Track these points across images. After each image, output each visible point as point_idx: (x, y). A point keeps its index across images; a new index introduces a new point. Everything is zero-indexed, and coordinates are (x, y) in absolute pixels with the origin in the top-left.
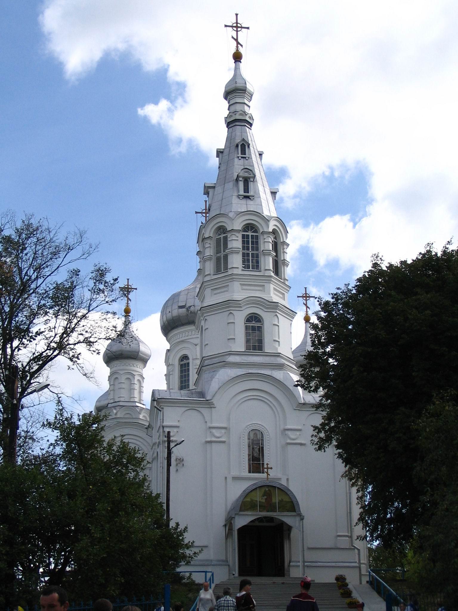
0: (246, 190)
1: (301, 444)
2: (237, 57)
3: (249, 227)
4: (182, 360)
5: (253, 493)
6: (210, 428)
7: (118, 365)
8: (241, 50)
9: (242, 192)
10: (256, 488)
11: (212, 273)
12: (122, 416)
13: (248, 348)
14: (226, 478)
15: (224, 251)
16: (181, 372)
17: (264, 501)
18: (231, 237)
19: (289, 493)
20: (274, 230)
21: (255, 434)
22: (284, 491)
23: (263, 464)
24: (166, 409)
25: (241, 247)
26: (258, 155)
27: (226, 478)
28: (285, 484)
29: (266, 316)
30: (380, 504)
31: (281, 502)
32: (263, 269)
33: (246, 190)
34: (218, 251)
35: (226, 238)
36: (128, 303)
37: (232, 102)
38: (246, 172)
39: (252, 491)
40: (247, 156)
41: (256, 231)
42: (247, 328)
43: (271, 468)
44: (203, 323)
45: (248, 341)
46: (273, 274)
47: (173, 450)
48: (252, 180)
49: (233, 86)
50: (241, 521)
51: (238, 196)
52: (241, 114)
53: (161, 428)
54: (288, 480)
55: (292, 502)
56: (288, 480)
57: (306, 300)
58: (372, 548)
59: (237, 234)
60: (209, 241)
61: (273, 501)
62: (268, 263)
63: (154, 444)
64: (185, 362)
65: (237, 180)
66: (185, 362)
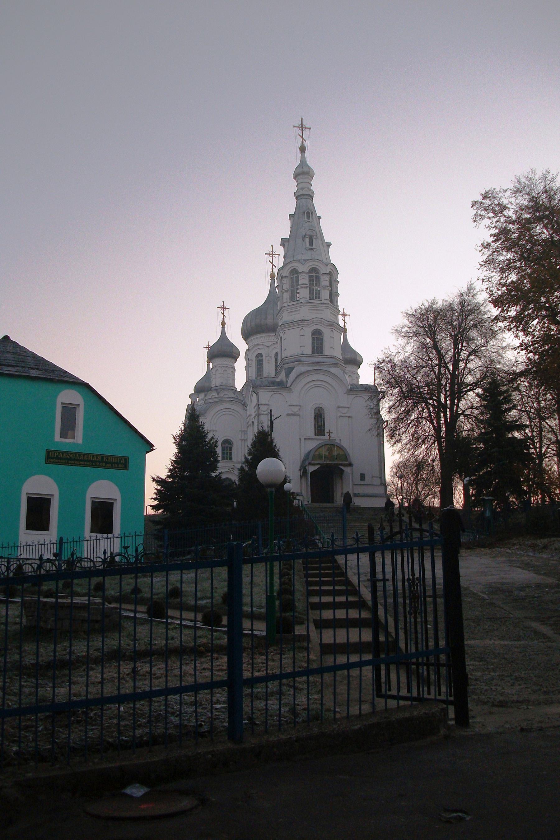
0: (311, 244)
1: (349, 417)
2: (303, 149)
3: (314, 270)
4: (258, 357)
5: (320, 449)
6: (290, 405)
7: (219, 361)
8: (306, 144)
9: (308, 245)
10: (322, 446)
11: (288, 302)
12: (222, 396)
13: (313, 352)
14: (300, 439)
15: (297, 286)
16: (257, 365)
17: (327, 454)
18: (301, 277)
19: (344, 449)
20: (330, 272)
21: (319, 410)
22: (340, 448)
23: (324, 430)
24: (260, 392)
25: (308, 284)
26: (318, 220)
27: (300, 439)
28: (339, 442)
29: (327, 333)
30: (523, 478)
31: (338, 455)
32: (323, 299)
33: (311, 244)
34: (292, 286)
35: (297, 277)
36: (223, 318)
37: (299, 181)
38: (311, 232)
39: (319, 448)
40: (311, 220)
41: (318, 273)
42: (313, 339)
43: (332, 433)
44: (282, 335)
45: (313, 348)
46: (329, 303)
47: (274, 421)
48: (315, 237)
49: (300, 170)
50: (311, 469)
51: (306, 248)
52: (306, 191)
53: (258, 405)
54: (340, 440)
55: (346, 455)
56: (340, 440)
57: (344, 317)
58: (440, 491)
59: (306, 275)
60: (286, 279)
61: (333, 454)
62: (325, 295)
63: (250, 416)
64: (260, 358)
65: (305, 236)
66: (260, 358)
